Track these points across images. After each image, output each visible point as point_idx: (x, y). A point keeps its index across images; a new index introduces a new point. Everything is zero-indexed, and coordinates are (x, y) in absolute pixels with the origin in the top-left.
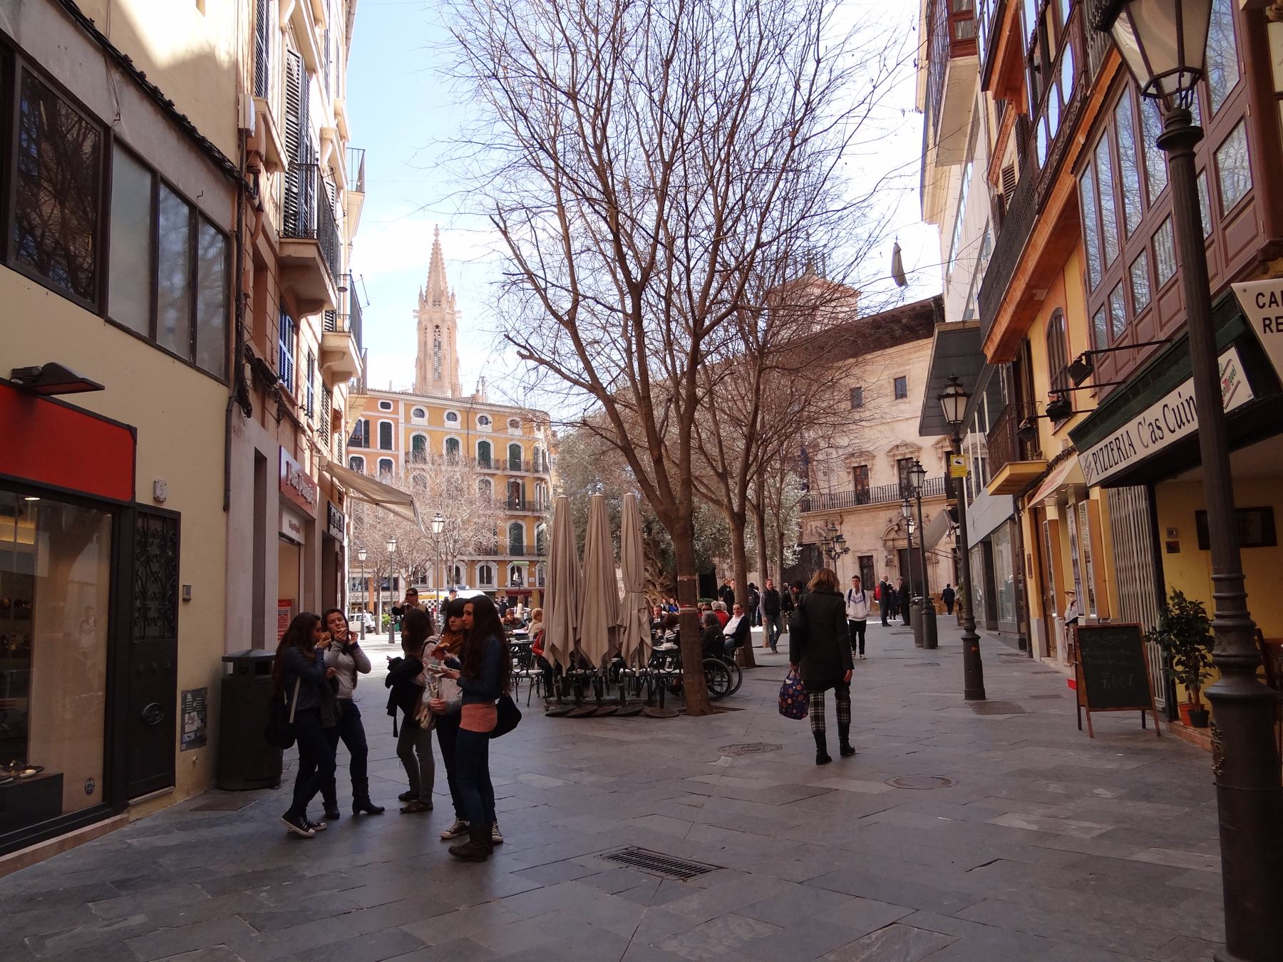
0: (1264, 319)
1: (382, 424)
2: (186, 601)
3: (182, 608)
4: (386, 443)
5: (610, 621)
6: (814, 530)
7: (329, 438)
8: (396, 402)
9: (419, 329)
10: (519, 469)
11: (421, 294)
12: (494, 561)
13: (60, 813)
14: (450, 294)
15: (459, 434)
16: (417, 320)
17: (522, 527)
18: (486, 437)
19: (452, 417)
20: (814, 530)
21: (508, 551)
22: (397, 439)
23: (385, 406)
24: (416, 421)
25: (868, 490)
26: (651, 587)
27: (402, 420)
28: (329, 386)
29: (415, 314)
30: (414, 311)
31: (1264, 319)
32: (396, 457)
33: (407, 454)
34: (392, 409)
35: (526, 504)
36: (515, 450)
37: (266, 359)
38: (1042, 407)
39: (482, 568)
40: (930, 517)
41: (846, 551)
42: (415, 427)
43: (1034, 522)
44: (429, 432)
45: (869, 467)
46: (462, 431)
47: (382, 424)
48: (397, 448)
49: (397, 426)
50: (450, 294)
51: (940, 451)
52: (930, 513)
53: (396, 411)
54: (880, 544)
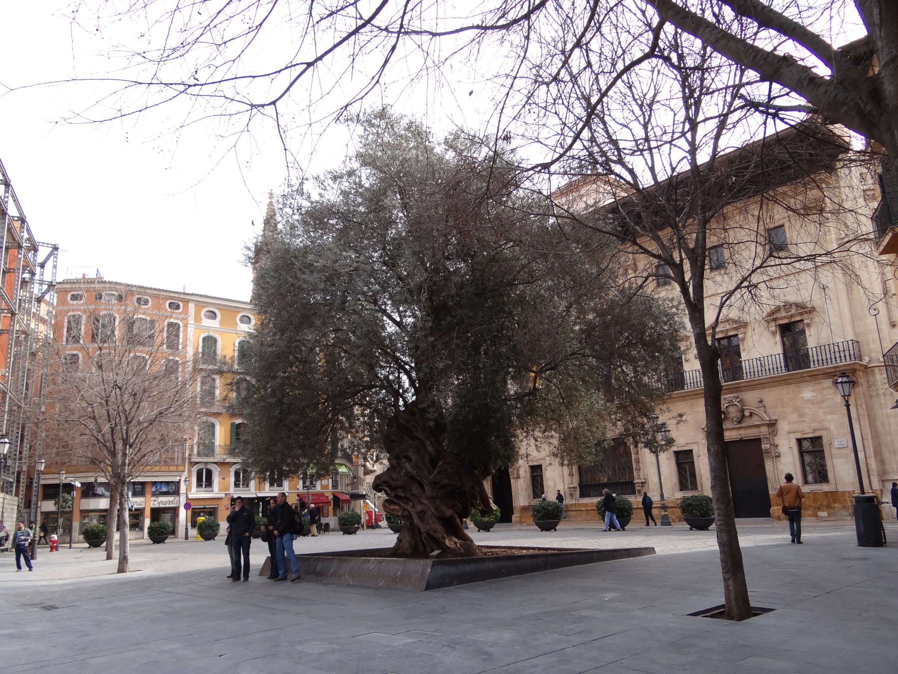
5: (12, 570)
12: (216, 463)
24: (207, 322)
26: (415, 489)
34: (180, 310)
40: (765, 403)
51: (773, 324)
52: (764, 398)
53: (186, 311)
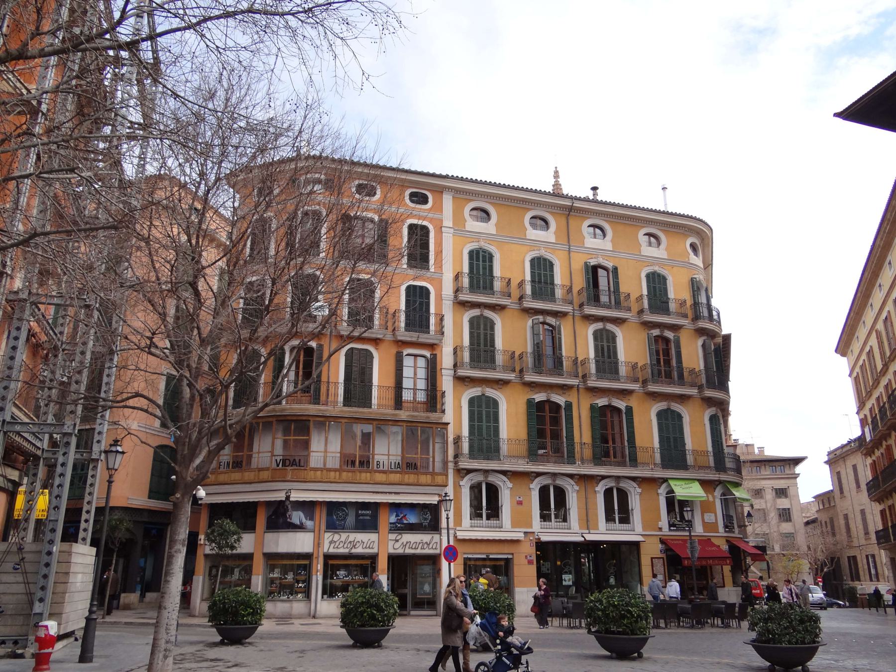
1: (412, 227)
10: (666, 311)
17: (551, 265)
18: (604, 257)
21: (658, 457)
22: (439, 253)
27: (448, 222)
34: (429, 205)
35: (686, 374)
36: (656, 282)
38: (746, 515)
39: (608, 493)
49: (439, 229)
53: (438, 207)
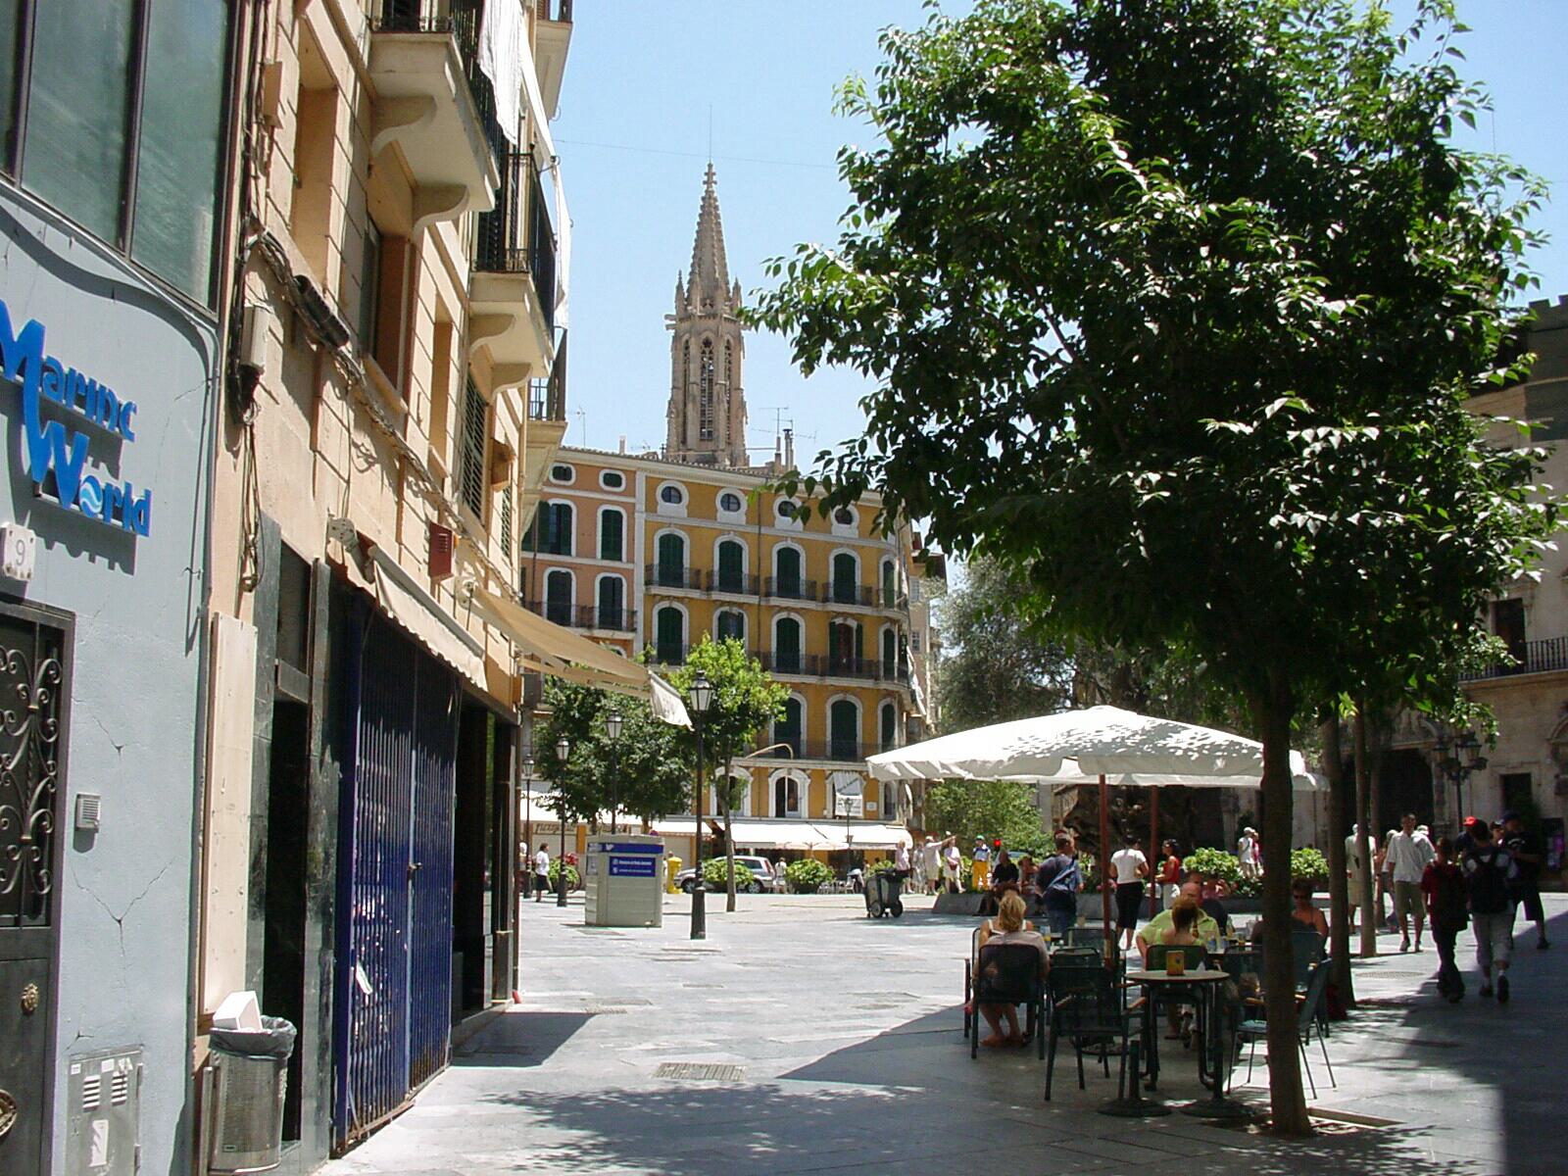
0: (611, 873)
1: (606, 513)
2: (85, 838)
3: (71, 860)
4: (612, 548)
6: (1415, 723)
7: (483, 493)
8: (631, 474)
9: (675, 348)
11: (680, 287)
13: (1526, 388)
14: (731, 286)
15: (742, 535)
16: (672, 332)
18: (793, 539)
19: (730, 502)
20: (1415, 723)
23: (613, 480)
25: (1525, 644)
27: (641, 506)
28: (483, 389)
29: (669, 322)
30: (667, 317)
31: (611, 873)
32: (630, 574)
33: (648, 568)
37: (325, 290)
41: (1480, 764)
42: (665, 520)
43: (53, 915)
44: (689, 529)
45: (1525, 602)
46: (749, 529)
47: (606, 513)
48: (631, 560)
50: (731, 286)
54: (1544, 752)
